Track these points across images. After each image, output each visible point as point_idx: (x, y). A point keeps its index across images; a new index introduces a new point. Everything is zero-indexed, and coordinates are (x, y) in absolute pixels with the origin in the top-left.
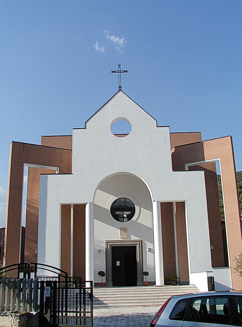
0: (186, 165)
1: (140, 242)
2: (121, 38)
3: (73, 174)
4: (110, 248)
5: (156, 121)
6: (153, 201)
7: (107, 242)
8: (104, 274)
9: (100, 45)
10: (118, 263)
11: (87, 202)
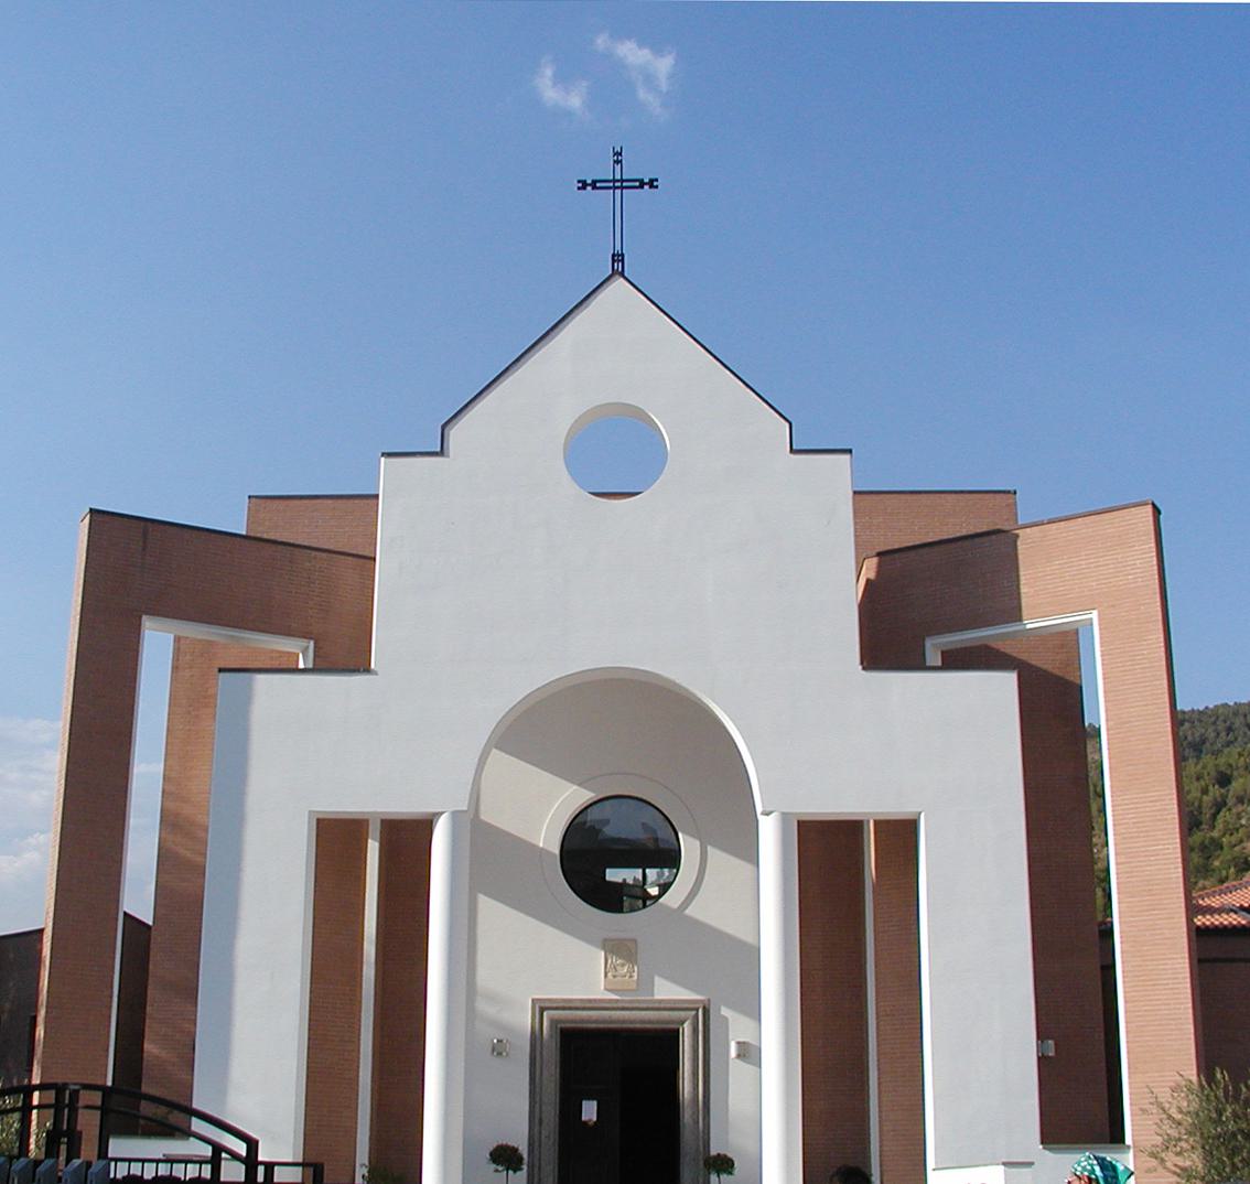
0: (929, 643)
1: (697, 1010)
2: (658, 51)
3: (376, 674)
4: (551, 1036)
5: (787, 425)
6: (762, 814)
7: (541, 1008)
8: (521, 1159)
9: (561, 79)
10: (590, 1111)
11: (440, 810)
